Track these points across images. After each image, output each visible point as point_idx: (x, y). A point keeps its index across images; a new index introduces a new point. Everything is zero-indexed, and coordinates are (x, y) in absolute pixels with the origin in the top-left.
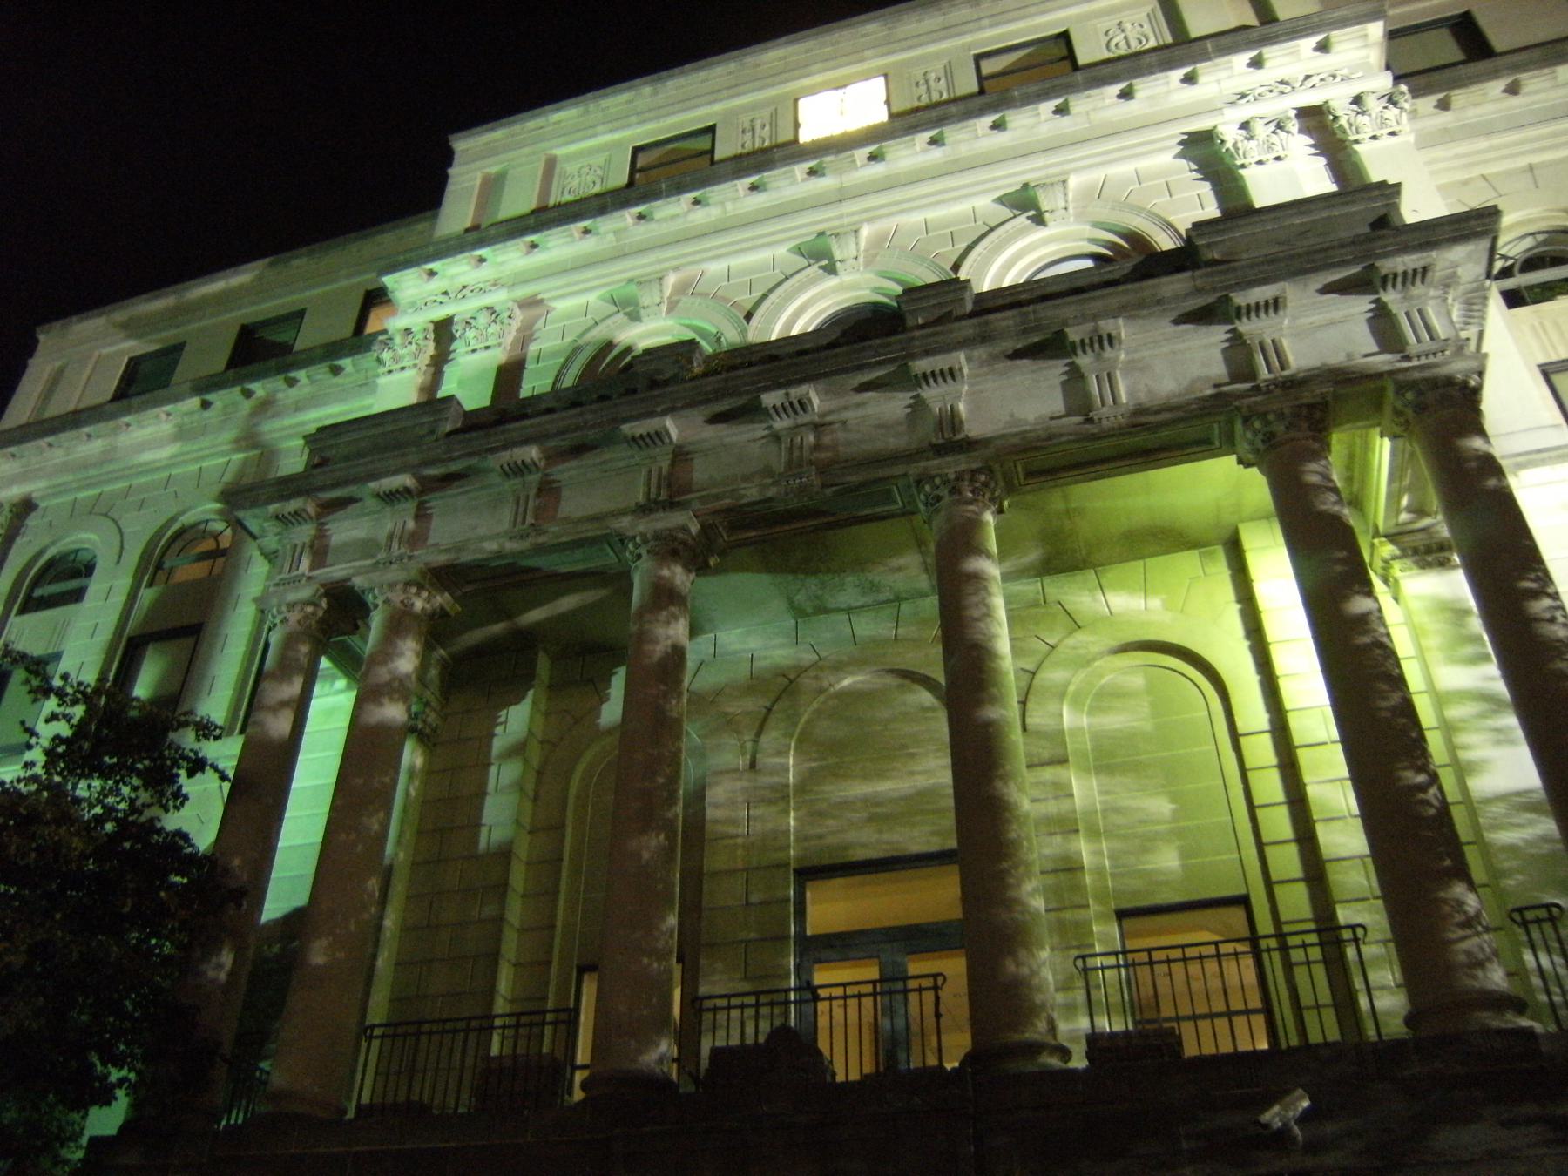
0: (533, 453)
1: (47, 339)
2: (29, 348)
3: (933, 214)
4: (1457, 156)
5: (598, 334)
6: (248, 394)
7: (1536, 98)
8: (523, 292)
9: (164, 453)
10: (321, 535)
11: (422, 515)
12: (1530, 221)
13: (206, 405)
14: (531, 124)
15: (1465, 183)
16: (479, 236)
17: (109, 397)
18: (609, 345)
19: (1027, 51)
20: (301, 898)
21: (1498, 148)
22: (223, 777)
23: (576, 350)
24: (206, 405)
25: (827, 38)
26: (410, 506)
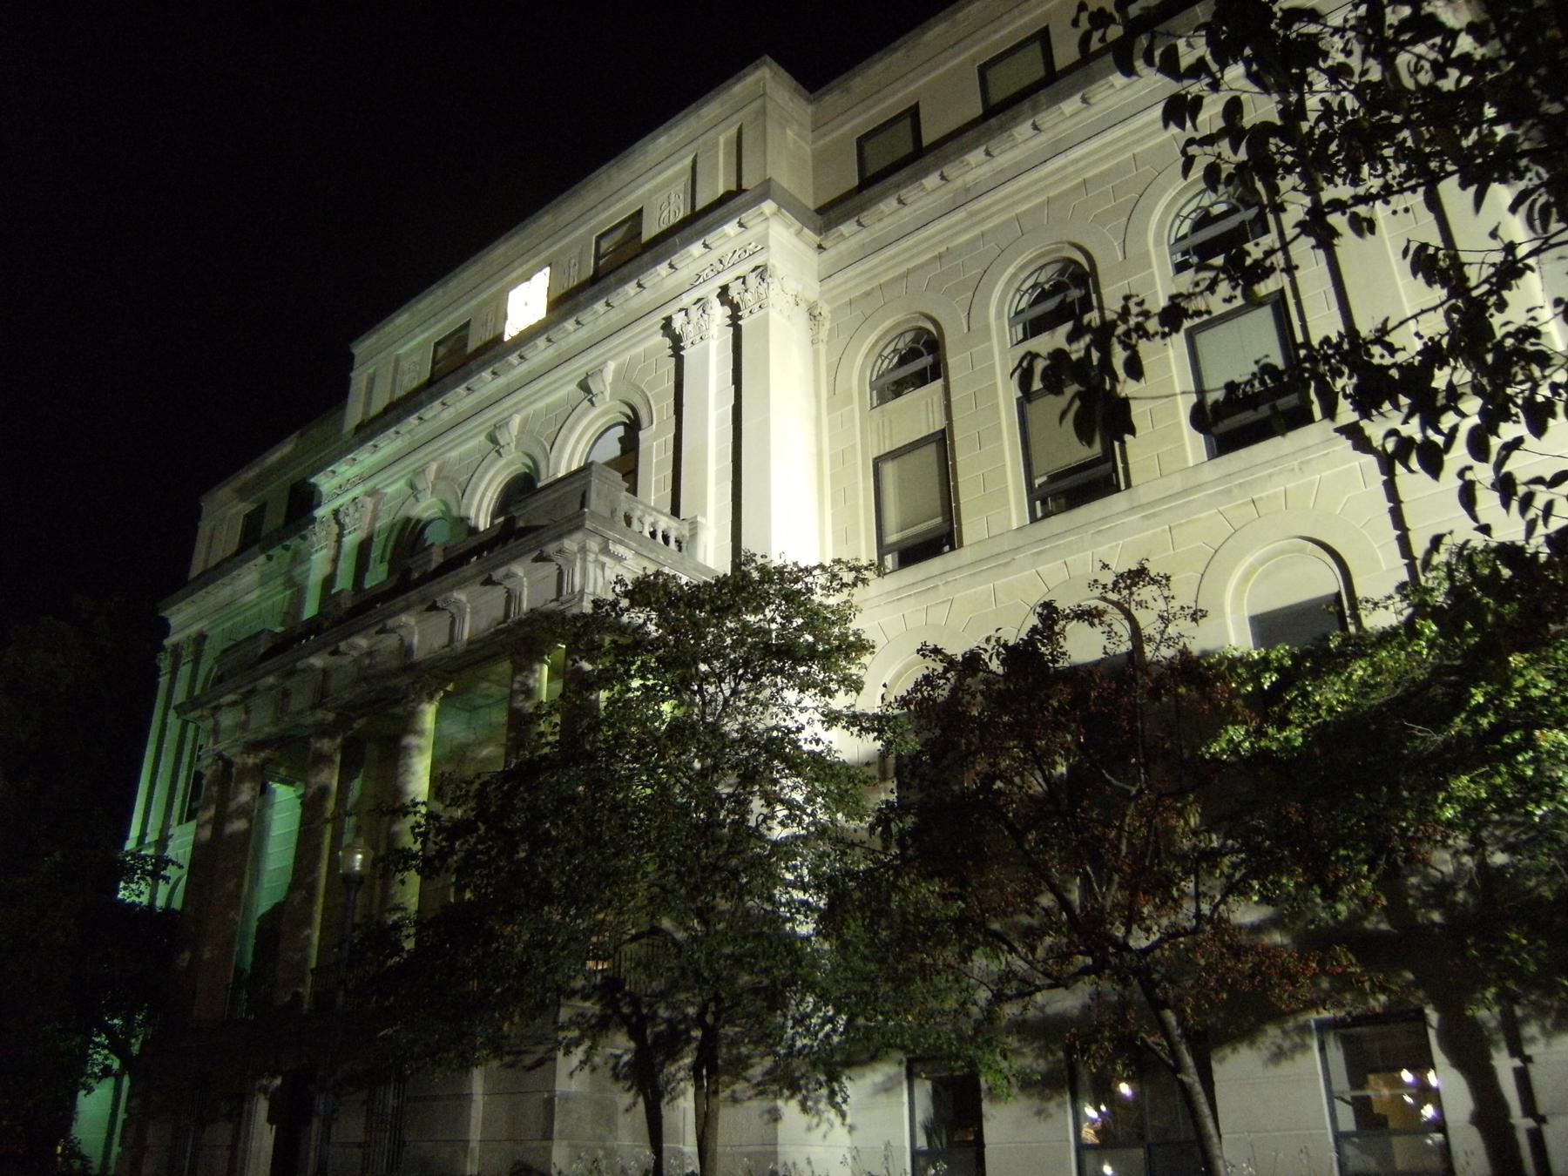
0: (271, 680)
1: (360, 349)
2: (348, 361)
3: (550, 400)
4: (862, 273)
5: (402, 513)
6: (287, 548)
7: (916, 206)
8: (370, 484)
9: (253, 596)
10: (217, 724)
11: (247, 712)
12: (898, 324)
13: (270, 558)
14: (387, 329)
15: (868, 294)
16: (370, 429)
17: (234, 548)
18: (408, 520)
19: (625, 228)
20: (279, 896)
21: (905, 250)
22: (181, 867)
23: (393, 526)
24: (270, 558)
25: (529, 231)
26: (241, 707)
